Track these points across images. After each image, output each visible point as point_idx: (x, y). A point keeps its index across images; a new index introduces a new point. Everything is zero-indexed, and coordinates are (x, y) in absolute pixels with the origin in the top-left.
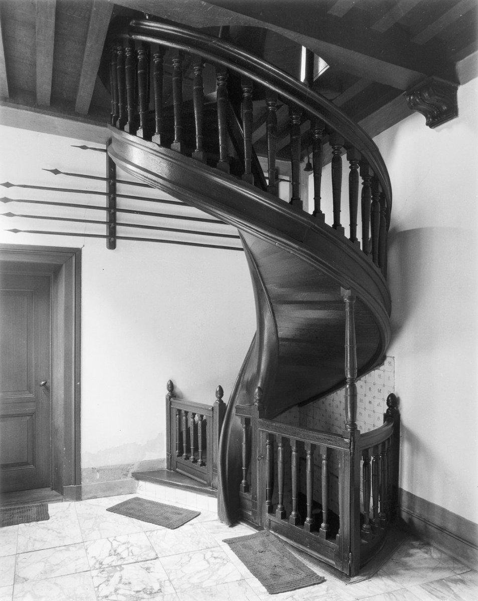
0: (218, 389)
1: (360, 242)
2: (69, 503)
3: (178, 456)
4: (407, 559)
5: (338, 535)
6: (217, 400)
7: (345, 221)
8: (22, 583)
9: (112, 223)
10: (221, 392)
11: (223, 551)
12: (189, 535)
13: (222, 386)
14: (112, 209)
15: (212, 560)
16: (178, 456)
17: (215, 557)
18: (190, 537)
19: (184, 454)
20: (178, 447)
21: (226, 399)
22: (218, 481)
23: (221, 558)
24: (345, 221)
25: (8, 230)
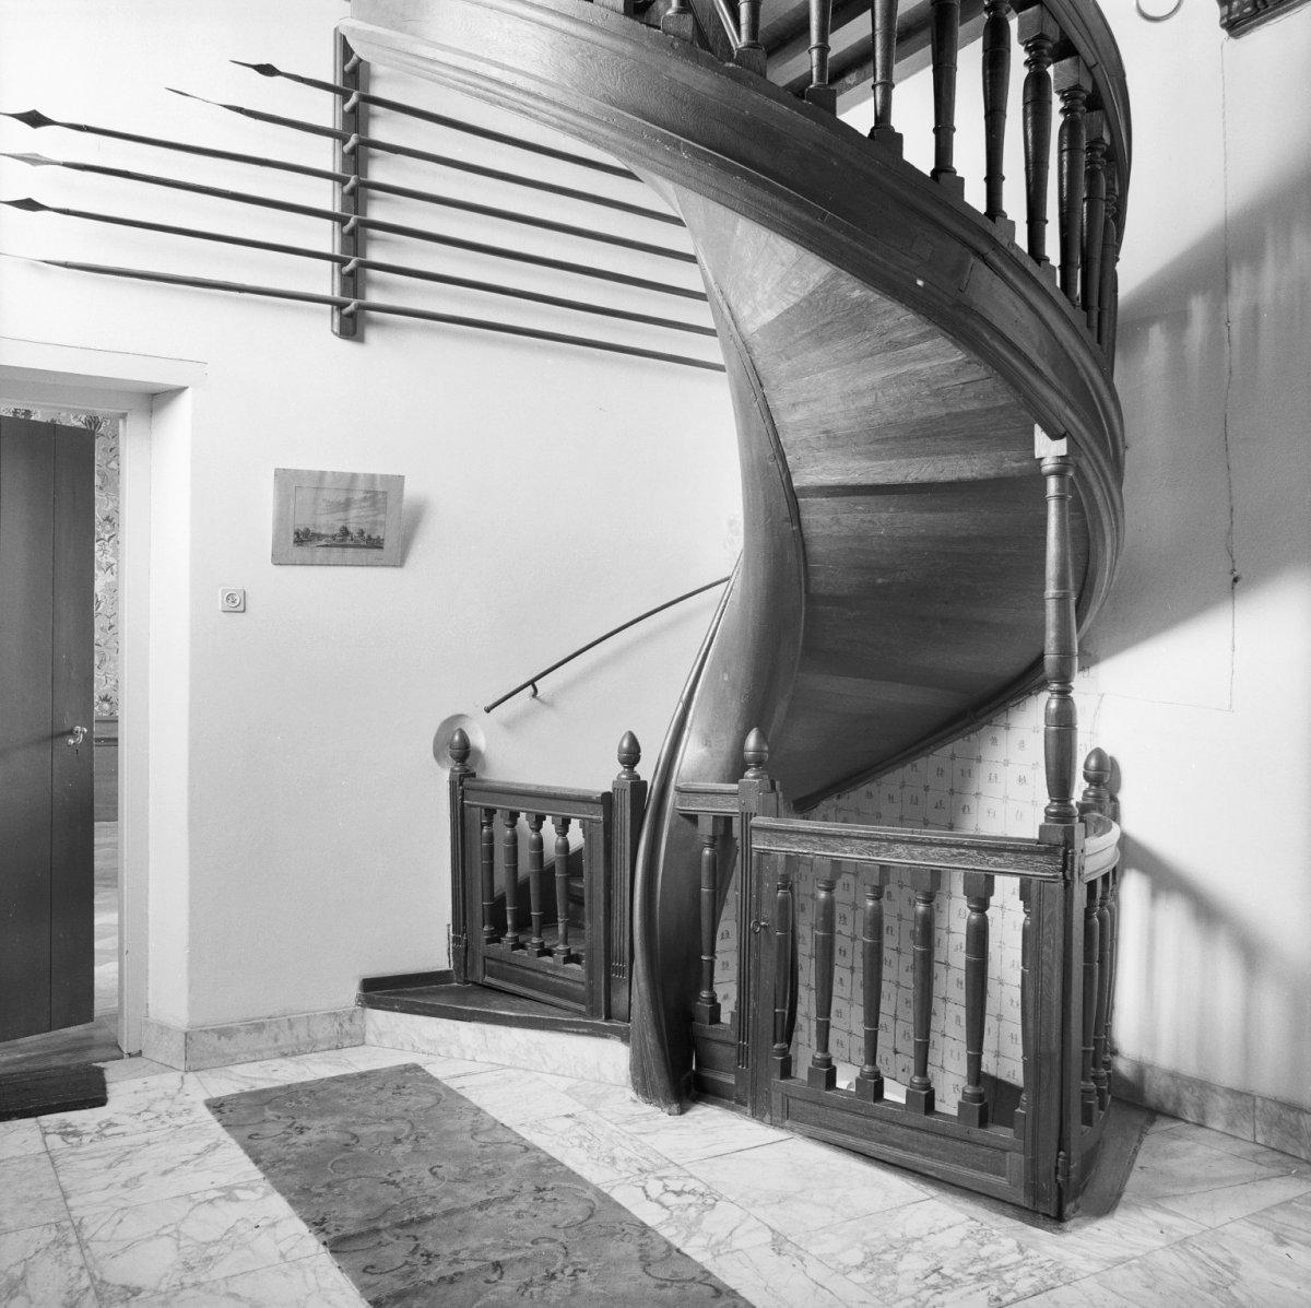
0: (625, 744)
1: (1054, 268)
2: (885, 949)
3: (489, 941)
4: (1173, 1163)
5: (1019, 1110)
6: (623, 773)
7: (1014, 204)
8: (122, 1301)
9: (353, 282)
10: (631, 756)
11: (691, 1177)
12: (576, 1142)
13: (635, 734)
14: (356, 231)
15: (670, 1199)
16: (489, 941)
17: (675, 1192)
18: (581, 1146)
19: (509, 935)
20: (487, 916)
21: (647, 770)
22: (637, 993)
23: (692, 1192)
24: (1014, 204)
25: (225, 106)
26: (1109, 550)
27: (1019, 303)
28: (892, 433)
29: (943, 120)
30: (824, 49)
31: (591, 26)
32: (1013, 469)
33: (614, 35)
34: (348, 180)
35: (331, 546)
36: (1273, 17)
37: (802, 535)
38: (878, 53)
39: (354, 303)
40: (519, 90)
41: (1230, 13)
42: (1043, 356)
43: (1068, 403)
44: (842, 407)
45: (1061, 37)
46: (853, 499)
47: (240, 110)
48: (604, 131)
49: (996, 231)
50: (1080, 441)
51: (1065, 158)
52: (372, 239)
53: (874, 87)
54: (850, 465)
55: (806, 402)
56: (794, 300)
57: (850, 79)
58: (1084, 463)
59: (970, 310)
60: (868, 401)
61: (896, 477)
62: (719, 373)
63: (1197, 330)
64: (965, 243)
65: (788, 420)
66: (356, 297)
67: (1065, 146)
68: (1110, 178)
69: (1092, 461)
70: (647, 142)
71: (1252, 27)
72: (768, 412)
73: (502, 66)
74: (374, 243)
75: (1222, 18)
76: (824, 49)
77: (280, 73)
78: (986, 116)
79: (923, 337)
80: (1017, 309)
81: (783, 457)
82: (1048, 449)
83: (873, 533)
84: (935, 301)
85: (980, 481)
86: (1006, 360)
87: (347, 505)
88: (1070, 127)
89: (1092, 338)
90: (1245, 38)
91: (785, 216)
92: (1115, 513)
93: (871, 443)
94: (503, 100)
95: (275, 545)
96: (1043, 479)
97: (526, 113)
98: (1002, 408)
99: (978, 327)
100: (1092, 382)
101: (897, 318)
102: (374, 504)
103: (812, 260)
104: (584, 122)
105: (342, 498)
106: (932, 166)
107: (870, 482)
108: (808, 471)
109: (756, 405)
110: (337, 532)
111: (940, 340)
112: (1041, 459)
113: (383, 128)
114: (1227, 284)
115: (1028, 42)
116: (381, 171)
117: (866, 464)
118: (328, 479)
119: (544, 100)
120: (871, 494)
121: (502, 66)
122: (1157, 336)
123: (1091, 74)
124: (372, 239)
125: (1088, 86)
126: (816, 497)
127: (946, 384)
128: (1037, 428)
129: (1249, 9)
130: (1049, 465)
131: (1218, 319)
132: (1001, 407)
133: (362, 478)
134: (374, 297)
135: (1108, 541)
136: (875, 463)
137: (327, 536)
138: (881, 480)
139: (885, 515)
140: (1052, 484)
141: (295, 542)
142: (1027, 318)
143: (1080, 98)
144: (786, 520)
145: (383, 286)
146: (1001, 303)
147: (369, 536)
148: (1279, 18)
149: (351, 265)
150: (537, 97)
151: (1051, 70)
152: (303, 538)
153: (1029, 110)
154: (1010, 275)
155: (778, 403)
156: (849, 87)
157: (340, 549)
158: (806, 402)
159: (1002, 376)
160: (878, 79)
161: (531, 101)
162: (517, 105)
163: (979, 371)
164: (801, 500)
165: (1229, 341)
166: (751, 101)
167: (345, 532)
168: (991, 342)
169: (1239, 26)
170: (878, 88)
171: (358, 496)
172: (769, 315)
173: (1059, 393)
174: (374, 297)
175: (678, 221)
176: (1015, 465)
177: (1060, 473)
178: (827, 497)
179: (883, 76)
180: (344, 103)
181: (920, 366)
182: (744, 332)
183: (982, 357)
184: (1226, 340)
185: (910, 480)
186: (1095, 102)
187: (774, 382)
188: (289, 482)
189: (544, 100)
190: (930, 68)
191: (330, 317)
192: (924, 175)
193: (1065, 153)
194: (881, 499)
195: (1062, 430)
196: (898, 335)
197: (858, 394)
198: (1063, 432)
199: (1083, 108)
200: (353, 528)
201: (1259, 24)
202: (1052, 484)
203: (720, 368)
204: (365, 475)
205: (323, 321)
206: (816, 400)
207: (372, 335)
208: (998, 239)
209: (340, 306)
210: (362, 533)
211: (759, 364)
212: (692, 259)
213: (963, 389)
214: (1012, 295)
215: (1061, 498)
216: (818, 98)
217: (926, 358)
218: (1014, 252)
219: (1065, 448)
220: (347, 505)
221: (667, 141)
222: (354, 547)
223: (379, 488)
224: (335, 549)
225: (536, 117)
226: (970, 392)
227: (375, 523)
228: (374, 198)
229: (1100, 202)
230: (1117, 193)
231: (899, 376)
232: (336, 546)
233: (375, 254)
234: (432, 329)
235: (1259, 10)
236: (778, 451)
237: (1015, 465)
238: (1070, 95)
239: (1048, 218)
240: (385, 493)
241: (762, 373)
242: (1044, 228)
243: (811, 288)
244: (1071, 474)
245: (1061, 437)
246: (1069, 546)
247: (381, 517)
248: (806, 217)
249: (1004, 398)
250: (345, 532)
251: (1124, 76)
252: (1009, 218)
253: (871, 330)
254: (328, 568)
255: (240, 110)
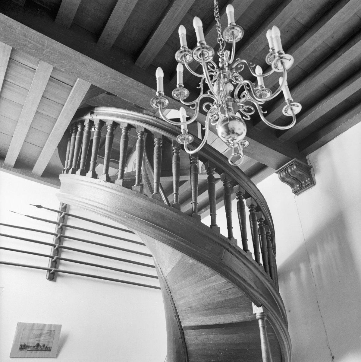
7: (237, 234)
9: (55, 263)
14: (58, 249)
24: (237, 234)
25: (25, 215)
26: (286, 347)
27: (241, 263)
28: (210, 307)
29: (212, 212)
30: (177, 194)
31: (116, 190)
32: (249, 318)
33: (119, 191)
34: (58, 235)
35: (33, 350)
36: (305, 190)
37: (185, 344)
38: (193, 195)
39: (53, 269)
40: (93, 206)
41: (294, 189)
42: (251, 280)
43: (261, 295)
44: (194, 299)
45: (246, 192)
46: (201, 330)
47: (30, 216)
48: (114, 216)
49: (231, 242)
50: (267, 307)
51: (252, 223)
52: (63, 251)
53: (192, 204)
54: (199, 318)
55: (184, 297)
56: (174, 264)
57: (203, 210)
58: (270, 315)
59: (224, 265)
60: (201, 297)
61: (213, 322)
62: (158, 290)
63: (303, 273)
64: (221, 246)
65: (178, 303)
66: (55, 268)
67: (251, 220)
68: (267, 229)
69: (273, 314)
70: (127, 219)
71: (301, 193)
72: (173, 301)
73: (89, 200)
74: (63, 252)
75: (293, 191)
76: (196, 203)
77: (43, 208)
78: (226, 212)
79: (213, 275)
80: (240, 265)
81: (178, 316)
82: (257, 311)
83: (208, 343)
84: (213, 262)
85: (239, 323)
86: (238, 281)
87: (40, 335)
88: (252, 216)
89: (268, 275)
90: (300, 196)
91: (166, 238)
92: (286, 334)
93: (204, 311)
94: (89, 209)
95: (12, 351)
96: (257, 321)
97: (94, 212)
98: (241, 297)
99: (227, 270)
100: (270, 289)
101: (204, 270)
102: (50, 335)
103: (176, 252)
104: (109, 214)
105: (39, 333)
106: (210, 224)
107: (205, 324)
108: (186, 321)
109: (169, 299)
110: (35, 345)
111: (217, 275)
112: (255, 314)
113: (71, 222)
114: (309, 259)
115: (237, 193)
116: (69, 233)
117: (203, 318)
118: (35, 327)
119: (99, 208)
120: (206, 329)
121: (89, 200)
122: (292, 275)
123: (256, 202)
124: (63, 251)
125: (255, 204)
126: (189, 330)
127: (223, 290)
128: (253, 304)
129: (299, 188)
130: (258, 316)
131: (309, 270)
132: (241, 296)
133: (47, 325)
134: (61, 268)
135: (285, 343)
136: (206, 318)
137: (31, 346)
138: (209, 323)
139: (212, 336)
140: (260, 322)
141: (20, 349)
142: (245, 269)
143: (254, 208)
144: (180, 338)
145: (65, 265)
146: (237, 265)
147: (47, 347)
148: (307, 190)
149: (55, 259)
150: (97, 207)
151: (244, 200)
152: (23, 347)
153: (239, 210)
154: (240, 258)
155: (175, 298)
156: (203, 212)
157: (35, 351)
158: (184, 297)
159: (237, 286)
160: (193, 201)
161: (96, 208)
162: (92, 210)
163: (230, 285)
164: (184, 331)
165: (313, 276)
166: (156, 207)
167: (38, 345)
168: (232, 275)
169: (297, 192)
170: (193, 204)
171: (45, 332)
172: (169, 270)
173: (257, 291)
174: (61, 268)
175: (143, 244)
176: (249, 317)
177: (262, 319)
178: (193, 330)
179: (194, 201)
180: (61, 215)
181: (214, 284)
182: (164, 276)
183: (230, 280)
184: (312, 276)
185: (217, 323)
186: (258, 209)
187: (174, 292)
188: (21, 327)
189: (99, 208)
190: (224, 207)
191: (46, 274)
192: (208, 227)
193: (252, 222)
194: (210, 330)
195: (261, 304)
196: (205, 274)
197: (198, 294)
198: (261, 305)
199: (255, 210)
200: (41, 344)
201: (303, 192)
202: (260, 322)
203: (159, 288)
204: (48, 324)
205: (45, 274)
206: (186, 297)
207: (59, 279)
208: (232, 244)
209: (50, 270)
210: (44, 345)
211: (169, 286)
212: (151, 256)
213: (228, 291)
214: (238, 261)
215: (264, 328)
216: (194, 215)
217: (215, 281)
218: (237, 248)
219: (262, 310)
220: (40, 335)
221: (132, 218)
222: (40, 350)
223: (53, 329)
224: (34, 352)
225: (97, 213)
226: (230, 291)
227: (49, 342)
228: (65, 240)
229: (265, 235)
230: (270, 233)
231: (208, 288)
232: (35, 350)
233: (63, 256)
234: (78, 278)
235: (301, 189)
236: (176, 314)
237: (249, 317)
238: (251, 207)
239: (248, 239)
240: (54, 331)
241: (171, 289)
242: (247, 242)
243: (178, 260)
244: (266, 319)
245: (261, 306)
246: (268, 345)
247: (52, 340)
248: (172, 238)
249: (241, 294)
250: (38, 345)
251: (266, 203)
252: (235, 238)
253: (198, 273)
254: (37, 359)
255: (30, 216)
